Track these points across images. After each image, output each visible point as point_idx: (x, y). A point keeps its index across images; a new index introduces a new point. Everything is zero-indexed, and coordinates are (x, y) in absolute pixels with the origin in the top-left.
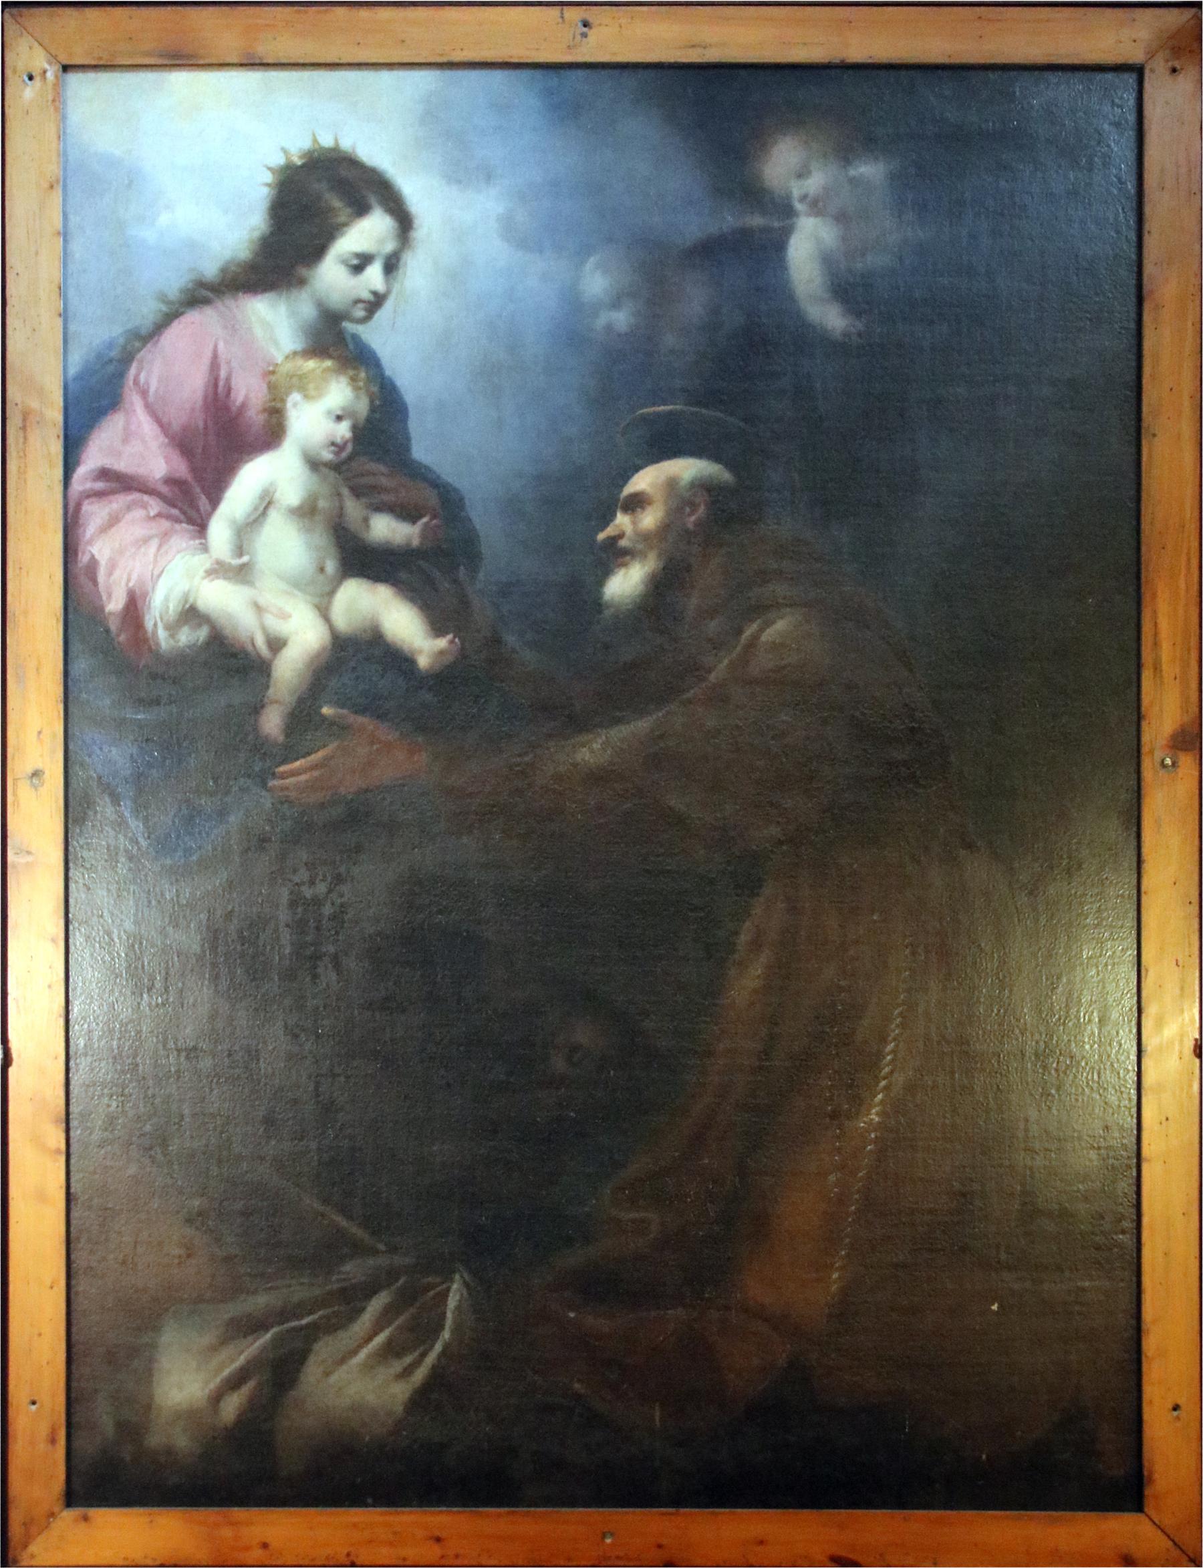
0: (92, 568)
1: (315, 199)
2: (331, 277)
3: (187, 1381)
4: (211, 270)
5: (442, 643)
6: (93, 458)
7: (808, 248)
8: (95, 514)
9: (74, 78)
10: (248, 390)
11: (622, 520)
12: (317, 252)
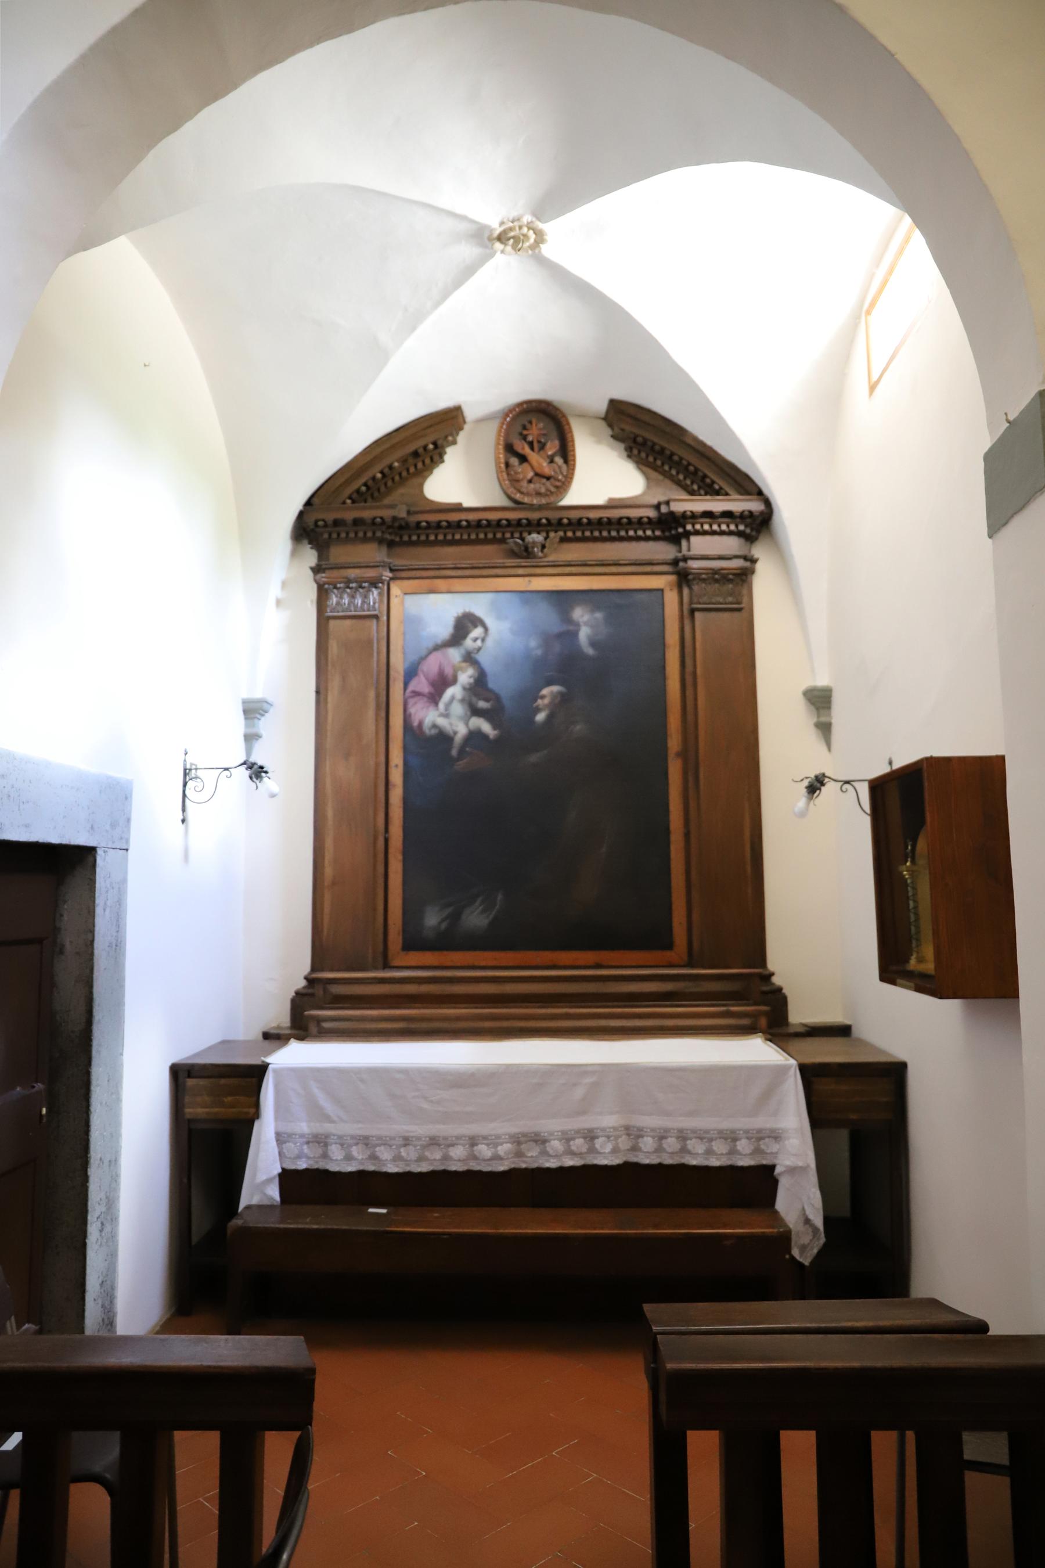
0: (410, 715)
1: (465, 624)
2: (469, 643)
3: (432, 919)
4: (439, 642)
5: (496, 732)
6: (412, 687)
7: (584, 634)
8: (411, 702)
9: (407, 597)
10: (448, 671)
11: (540, 702)
12: (465, 637)
